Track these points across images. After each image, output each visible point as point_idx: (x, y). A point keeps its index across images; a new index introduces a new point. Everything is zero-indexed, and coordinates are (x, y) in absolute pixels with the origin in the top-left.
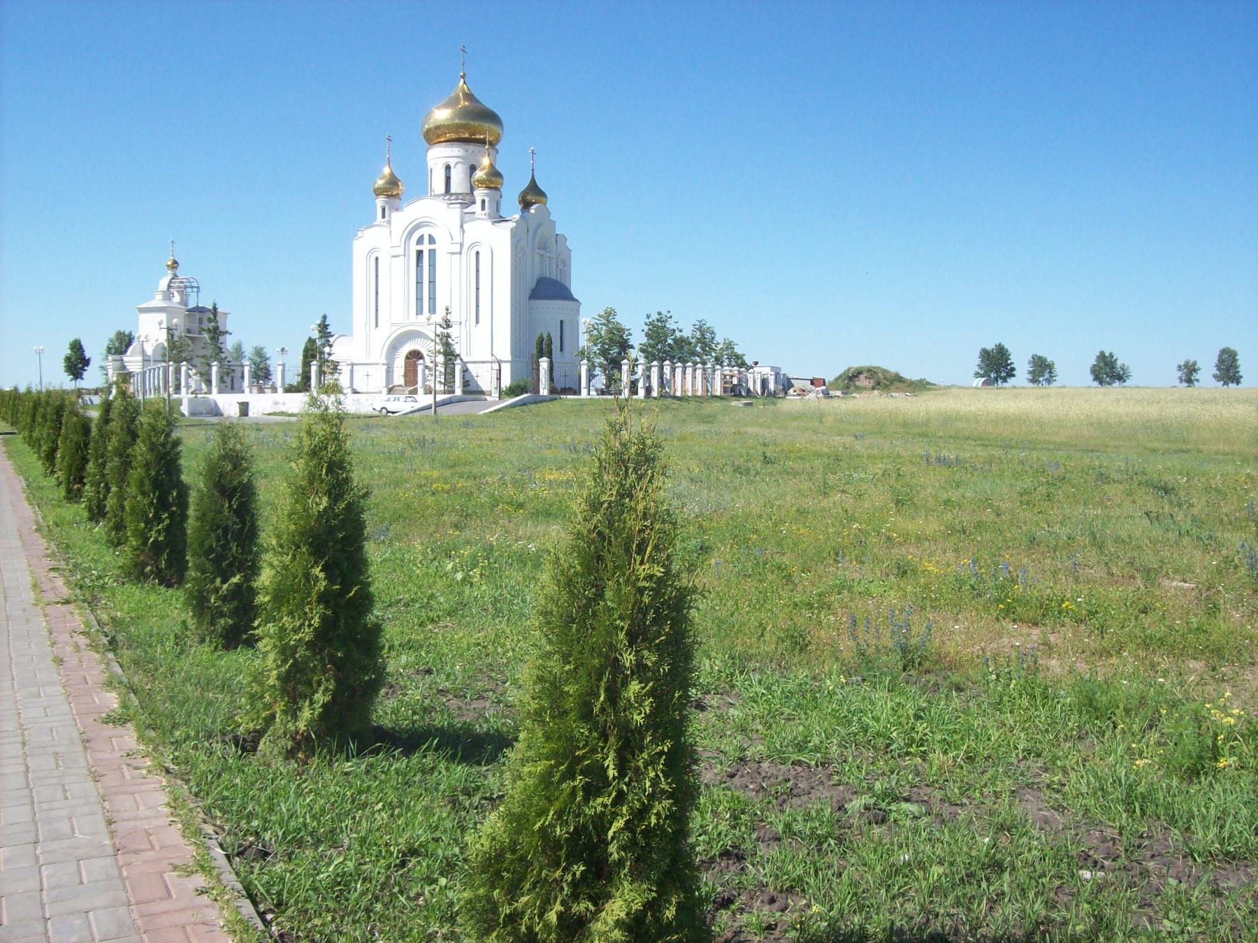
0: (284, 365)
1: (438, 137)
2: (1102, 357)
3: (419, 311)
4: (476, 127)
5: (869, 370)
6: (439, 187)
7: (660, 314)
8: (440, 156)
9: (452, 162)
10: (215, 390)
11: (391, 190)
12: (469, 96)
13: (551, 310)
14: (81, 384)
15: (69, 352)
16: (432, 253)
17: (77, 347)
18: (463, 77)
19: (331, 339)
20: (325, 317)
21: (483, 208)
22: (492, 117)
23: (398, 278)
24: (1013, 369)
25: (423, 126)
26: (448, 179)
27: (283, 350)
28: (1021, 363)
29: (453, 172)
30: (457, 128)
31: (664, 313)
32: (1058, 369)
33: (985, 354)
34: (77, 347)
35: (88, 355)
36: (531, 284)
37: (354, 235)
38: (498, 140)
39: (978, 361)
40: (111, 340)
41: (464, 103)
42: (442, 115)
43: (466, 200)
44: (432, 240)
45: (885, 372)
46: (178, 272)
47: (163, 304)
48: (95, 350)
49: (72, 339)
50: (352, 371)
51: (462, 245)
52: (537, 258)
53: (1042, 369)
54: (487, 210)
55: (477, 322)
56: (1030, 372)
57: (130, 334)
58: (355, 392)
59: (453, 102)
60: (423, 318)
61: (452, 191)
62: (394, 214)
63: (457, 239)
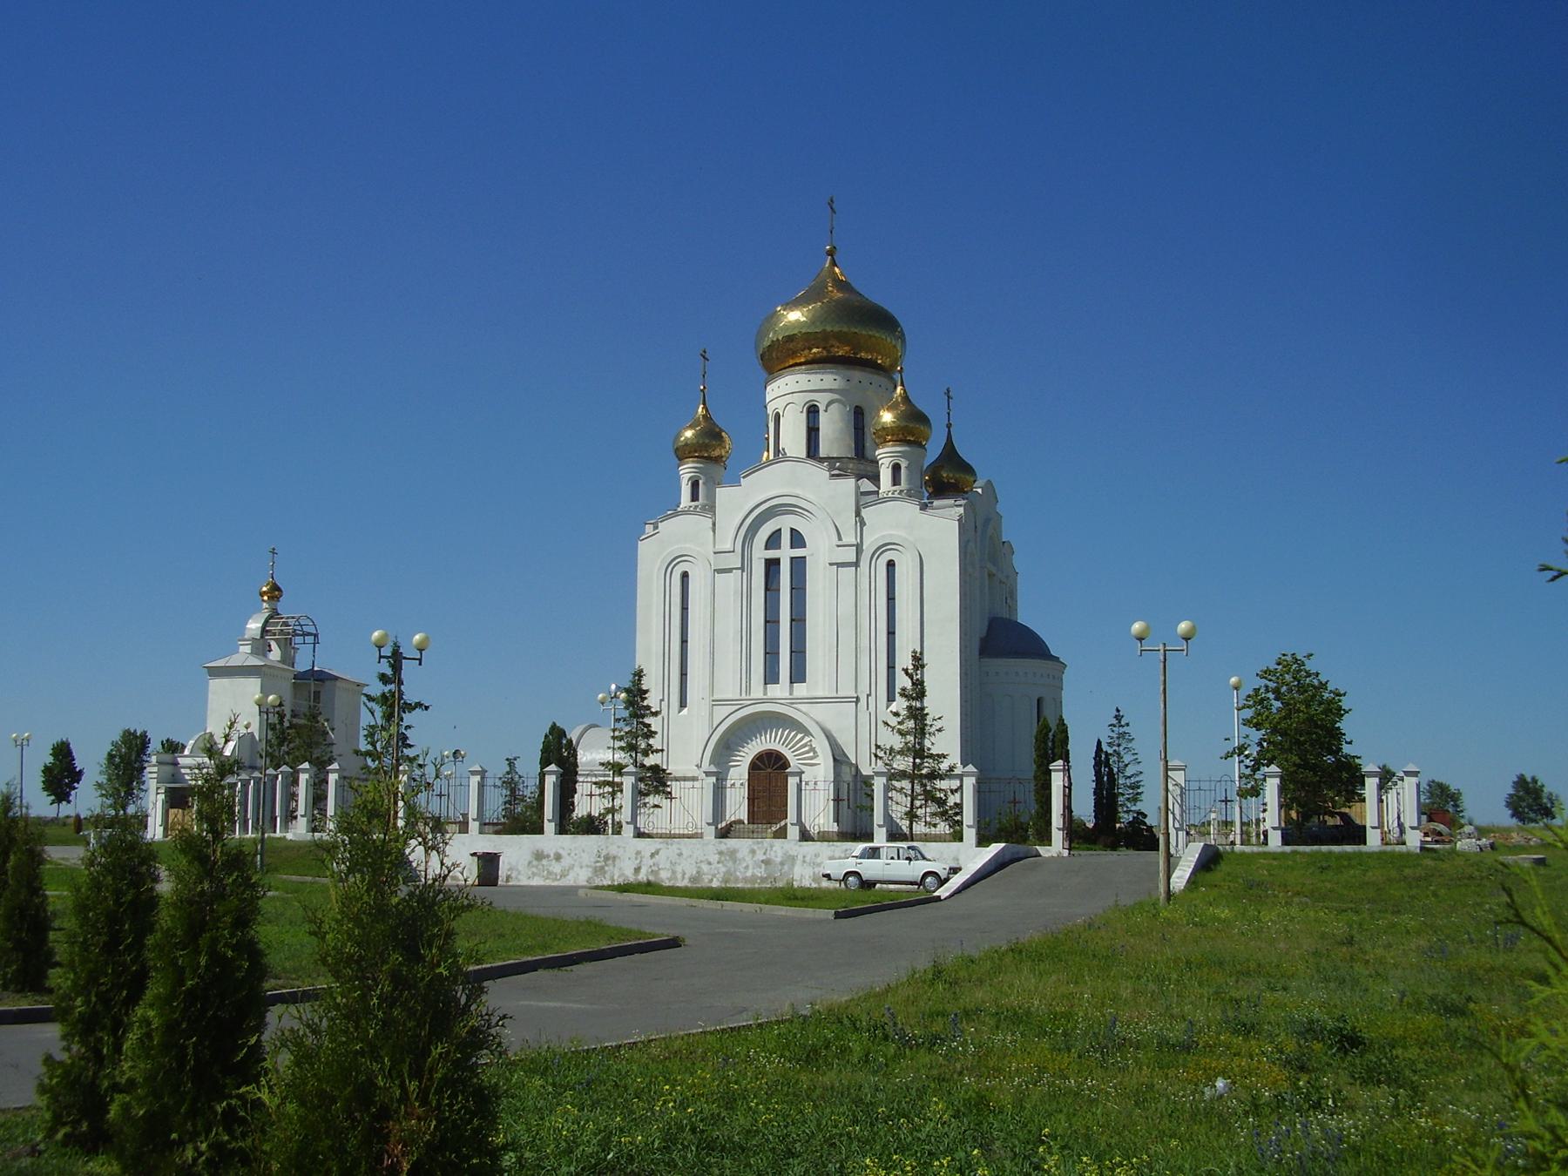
0: (483, 773)
1: (794, 354)
2: (1521, 783)
3: (771, 676)
4: (856, 339)
6: (793, 437)
8: (788, 394)
9: (822, 400)
11: (714, 453)
14: (66, 810)
15: (51, 759)
16: (798, 565)
17: (63, 752)
21: (896, 481)
22: (884, 321)
23: (727, 615)
25: (761, 334)
26: (813, 432)
29: (823, 418)
30: (821, 339)
34: (63, 752)
35: (79, 765)
36: (980, 629)
37: (637, 535)
44: (797, 539)
47: (255, 661)
48: (92, 761)
51: (859, 548)
54: (904, 485)
57: (144, 735)
58: (639, 835)
60: (779, 690)
61: (823, 453)
62: (722, 494)
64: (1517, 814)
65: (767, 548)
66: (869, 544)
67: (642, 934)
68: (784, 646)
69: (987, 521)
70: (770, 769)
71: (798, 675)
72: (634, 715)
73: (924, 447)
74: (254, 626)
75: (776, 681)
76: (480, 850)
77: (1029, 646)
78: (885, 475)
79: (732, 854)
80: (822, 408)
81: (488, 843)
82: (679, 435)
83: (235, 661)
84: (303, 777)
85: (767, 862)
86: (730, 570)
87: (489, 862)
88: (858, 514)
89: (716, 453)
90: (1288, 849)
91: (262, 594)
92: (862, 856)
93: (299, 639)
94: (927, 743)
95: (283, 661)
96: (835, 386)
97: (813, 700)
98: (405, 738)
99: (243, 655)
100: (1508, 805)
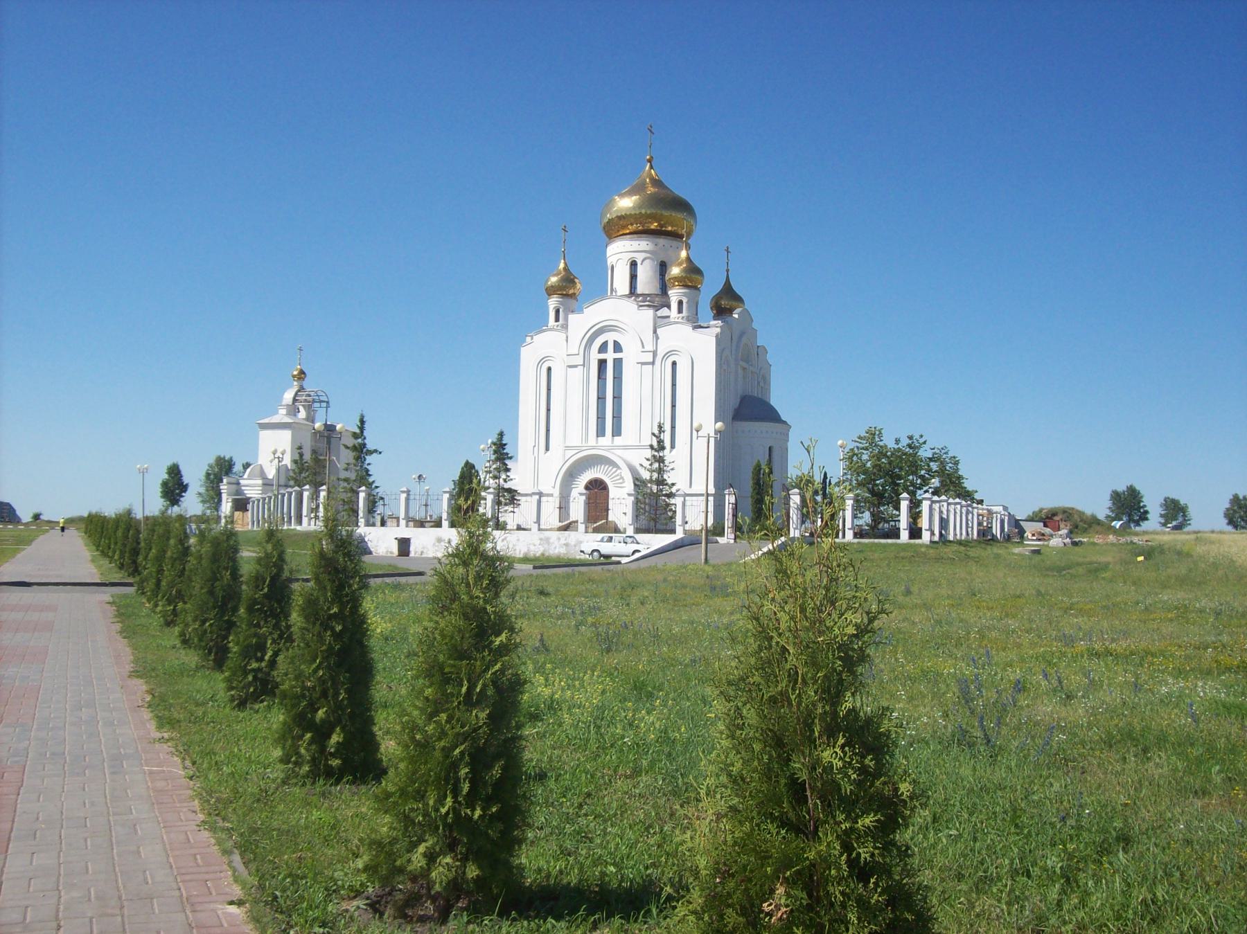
0: (408, 492)
1: (625, 227)
3: (601, 432)
4: (665, 218)
5: (1065, 511)
6: (621, 282)
7: (911, 438)
8: (621, 251)
9: (639, 258)
10: (362, 521)
11: (567, 289)
12: (656, 183)
13: (758, 430)
14: (175, 510)
15: (166, 476)
16: (618, 363)
17: (175, 471)
18: (649, 161)
19: (510, 464)
20: (501, 434)
21: (680, 311)
22: (682, 206)
23: (575, 393)
24: (1146, 512)
25: (603, 215)
26: (633, 277)
27: (420, 477)
28: (1153, 504)
29: (640, 269)
31: (916, 436)
32: (1192, 512)
33: (1116, 496)
34: (175, 471)
35: (186, 480)
36: (734, 402)
38: (689, 234)
39: (1109, 504)
40: (210, 466)
41: (651, 190)
42: (626, 203)
43: (659, 300)
44: (618, 347)
45: (1081, 514)
46: (306, 384)
48: (194, 478)
49: (169, 463)
50: (539, 502)
51: (655, 353)
52: (740, 371)
53: (1175, 512)
54: (685, 313)
55: (547, 449)
56: (1162, 516)
57: (231, 459)
59: (637, 189)
60: (606, 440)
61: (639, 291)
62: (571, 317)
63: (649, 346)
64: (1231, 522)
65: (600, 352)
66: (660, 354)
67: (395, 567)
68: (608, 415)
69: (742, 334)
70: (597, 489)
71: (617, 431)
72: (497, 459)
73: (698, 289)
74: (288, 396)
75: (604, 435)
76: (400, 536)
77: (771, 415)
78: (674, 306)
79: (547, 540)
80: (639, 262)
81: (404, 531)
82: (547, 280)
83: (275, 419)
84: (306, 494)
85: (567, 545)
86: (576, 366)
87: (404, 544)
88: (655, 332)
89: (571, 292)
90: (856, 541)
91: (294, 376)
92: (602, 540)
93: (317, 405)
94: (665, 477)
95: (307, 419)
96: (647, 248)
97: (626, 447)
98: (367, 471)
99: (281, 416)
100: (1226, 515)
